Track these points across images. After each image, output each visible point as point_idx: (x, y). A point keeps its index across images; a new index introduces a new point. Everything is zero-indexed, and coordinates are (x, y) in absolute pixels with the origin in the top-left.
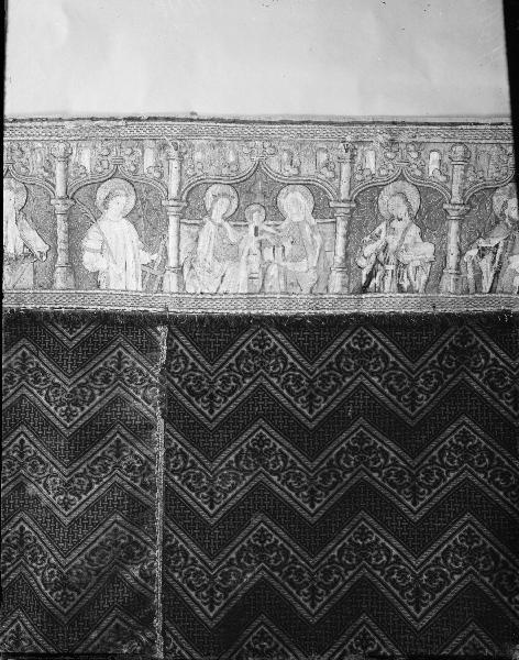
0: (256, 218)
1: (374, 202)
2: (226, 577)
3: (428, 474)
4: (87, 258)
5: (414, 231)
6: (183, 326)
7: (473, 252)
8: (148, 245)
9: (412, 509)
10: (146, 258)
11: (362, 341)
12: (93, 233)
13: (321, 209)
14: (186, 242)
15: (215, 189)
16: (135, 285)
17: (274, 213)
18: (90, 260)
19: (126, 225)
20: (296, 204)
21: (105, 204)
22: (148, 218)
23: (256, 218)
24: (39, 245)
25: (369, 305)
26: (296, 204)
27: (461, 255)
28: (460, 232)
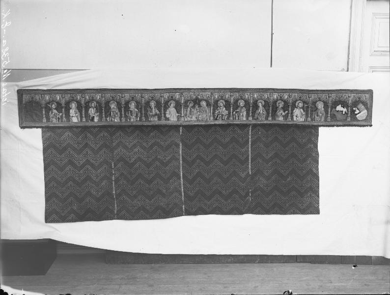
0: (197, 107)
1: (217, 104)
2: (86, 188)
3: (227, 135)
4: (167, 115)
5: (224, 108)
6: (185, 127)
7: (234, 113)
8: (178, 113)
9: (158, 163)
10: (177, 115)
11: (198, 129)
12: (168, 110)
13: (208, 105)
14: (185, 112)
15: (279, 102)
16: (176, 119)
17: (200, 106)
18: (168, 116)
19: (174, 109)
20: (204, 103)
21: (170, 105)
22: (178, 107)
23: (197, 107)
24: (158, 112)
25: (217, 122)
26: (204, 103)
27: (233, 113)
28: (233, 108)
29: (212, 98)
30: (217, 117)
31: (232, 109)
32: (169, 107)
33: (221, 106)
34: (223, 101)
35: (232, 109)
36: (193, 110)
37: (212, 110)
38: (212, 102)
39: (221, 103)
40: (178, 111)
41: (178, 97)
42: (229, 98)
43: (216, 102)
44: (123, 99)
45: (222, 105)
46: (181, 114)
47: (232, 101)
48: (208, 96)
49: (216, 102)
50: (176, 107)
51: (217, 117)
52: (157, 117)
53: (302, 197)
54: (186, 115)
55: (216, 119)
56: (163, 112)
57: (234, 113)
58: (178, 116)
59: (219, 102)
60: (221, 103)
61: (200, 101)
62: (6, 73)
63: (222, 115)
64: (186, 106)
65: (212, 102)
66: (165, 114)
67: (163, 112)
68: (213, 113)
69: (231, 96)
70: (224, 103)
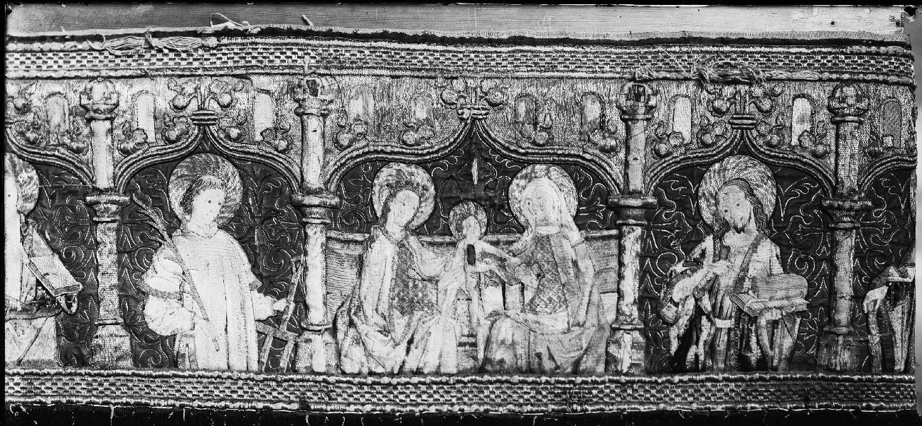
1: (687, 203)
5: (768, 251)
10: (266, 306)
13: (599, 209)
17: (503, 220)
19: (227, 245)
20: (546, 199)
21: (187, 202)
22: (269, 232)
23: (473, 228)
24: (60, 277)
26: (546, 199)
28: (858, 254)
29: (640, 133)
30: (688, 339)
31: (846, 261)
32: (174, 224)
33: (726, 226)
34: (755, 172)
35: (846, 261)
36: (428, 261)
37: (631, 260)
38: (637, 182)
39: (735, 196)
40: (274, 266)
41: (263, 118)
42: (817, 138)
43: (683, 177)
44: (32, 96)
45: (738, 208)
46: (301, 299)
47: (849, 172)
48: (593, 111)
49: (683, 177)
50: (236, 225)
51: (688, 339)
52: (48, 325)
53: (754, 277)
54: (352, 309)
55: (677, 364)
56: (107, 281)
57: (878, 294)
58: (277, 318)
59: (710, 184)
60: (735, 196)
61: (510, 166)
62: (847, 72)
63: (746, 319)
64: (356, 215)
65: (637, 182)
66: (133, 298)
67: (107, 281)
68: (649, 300)
69: (838, 119)
70: (767, 194)
